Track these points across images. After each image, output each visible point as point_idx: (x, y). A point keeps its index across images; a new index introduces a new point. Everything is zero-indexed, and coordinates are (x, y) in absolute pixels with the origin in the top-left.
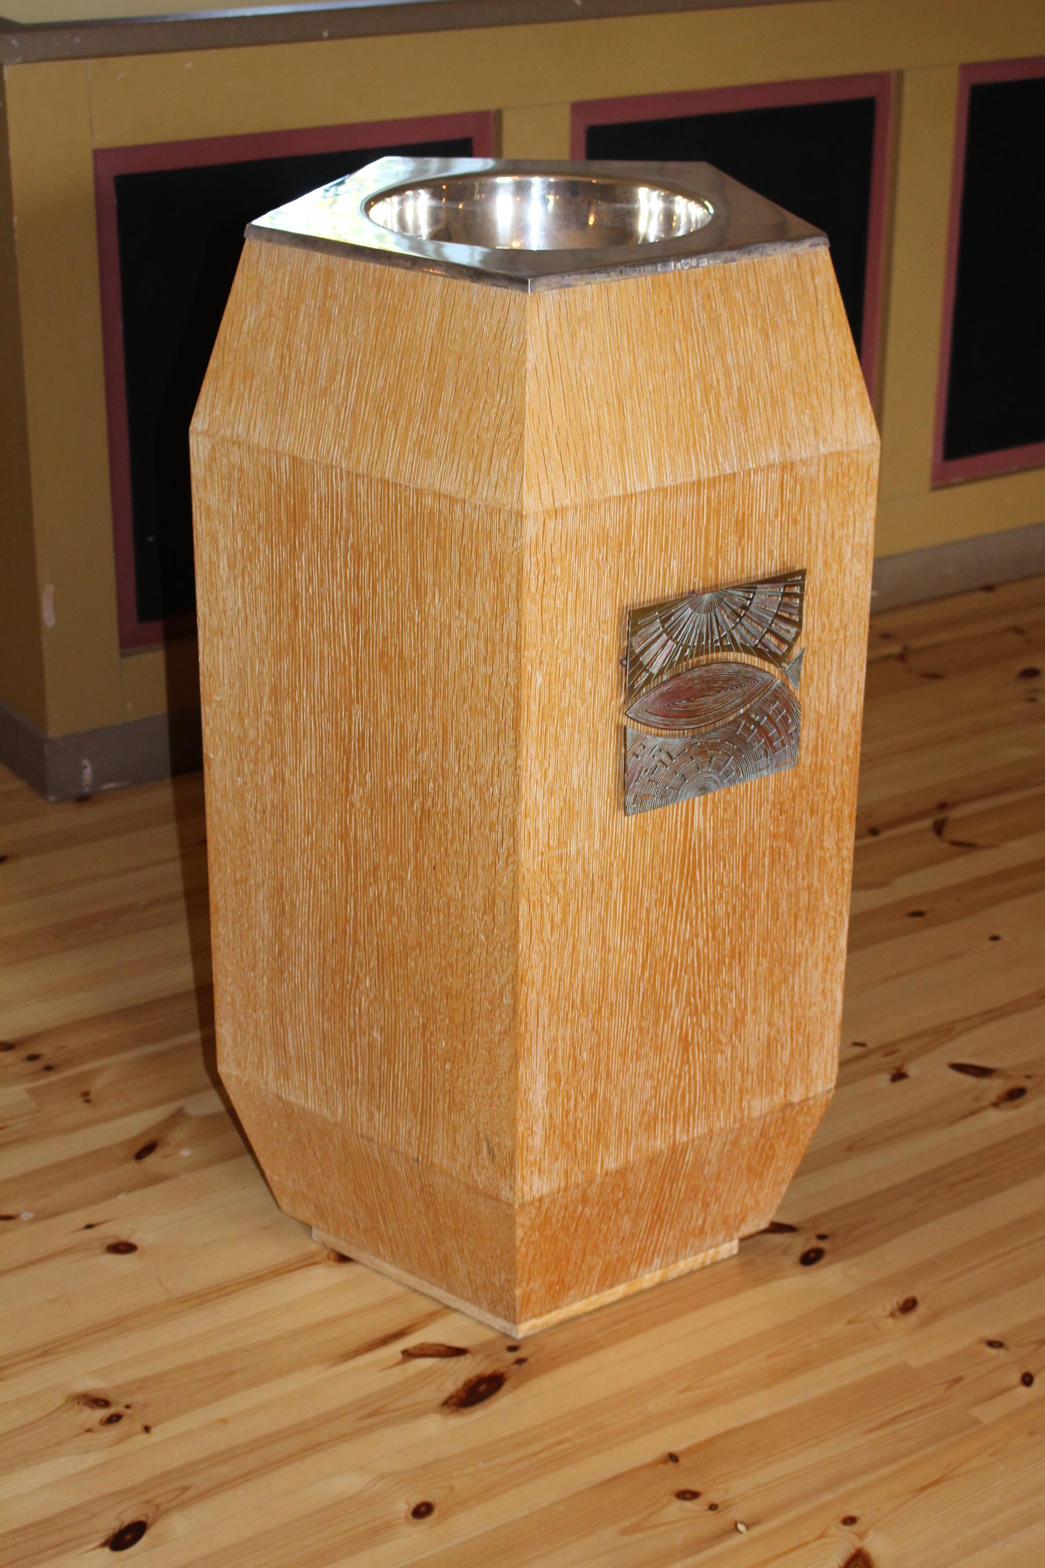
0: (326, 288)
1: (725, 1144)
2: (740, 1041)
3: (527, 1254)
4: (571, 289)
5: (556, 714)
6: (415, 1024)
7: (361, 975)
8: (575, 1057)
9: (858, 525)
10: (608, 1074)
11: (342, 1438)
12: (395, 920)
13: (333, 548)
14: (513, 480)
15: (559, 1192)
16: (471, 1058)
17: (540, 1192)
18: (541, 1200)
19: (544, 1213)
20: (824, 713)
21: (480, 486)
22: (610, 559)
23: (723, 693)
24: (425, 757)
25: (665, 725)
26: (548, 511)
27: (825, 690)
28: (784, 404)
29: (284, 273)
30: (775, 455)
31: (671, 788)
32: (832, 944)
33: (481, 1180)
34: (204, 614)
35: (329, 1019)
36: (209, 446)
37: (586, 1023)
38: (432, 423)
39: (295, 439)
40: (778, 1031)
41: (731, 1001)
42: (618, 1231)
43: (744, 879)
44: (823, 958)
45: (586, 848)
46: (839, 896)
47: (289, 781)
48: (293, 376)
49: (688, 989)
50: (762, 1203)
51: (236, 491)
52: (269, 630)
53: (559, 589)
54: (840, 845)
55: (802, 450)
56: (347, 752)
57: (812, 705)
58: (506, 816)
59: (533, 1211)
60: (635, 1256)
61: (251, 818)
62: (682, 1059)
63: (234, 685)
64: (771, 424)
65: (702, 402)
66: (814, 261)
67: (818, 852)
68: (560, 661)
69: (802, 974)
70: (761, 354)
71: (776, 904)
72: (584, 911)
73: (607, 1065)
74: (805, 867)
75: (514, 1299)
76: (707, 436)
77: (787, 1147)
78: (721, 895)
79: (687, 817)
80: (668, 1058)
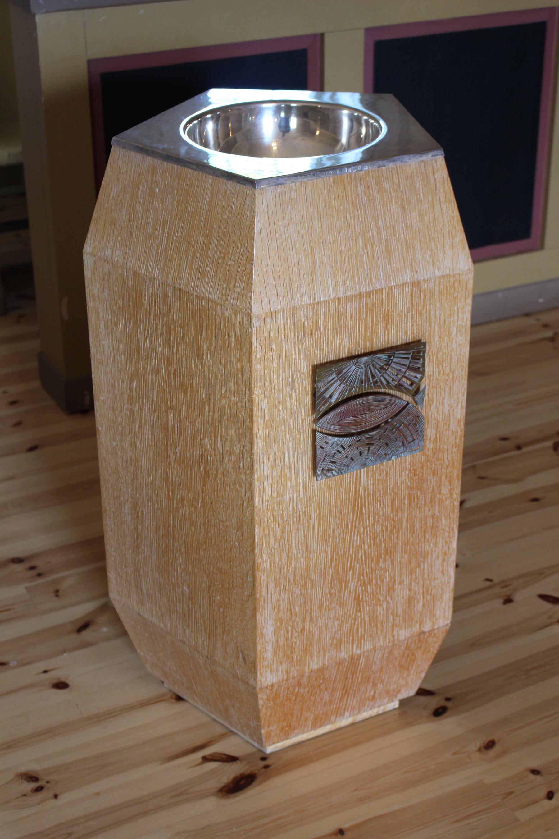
0: (152, 177)
1: (384, 654)
2: (392, 599)
3: (266, 713)
4: (283, 186)
5: (274, 425)
6: (204, 585)
7: (177, 555)
8: (291, 610)
9: (460, 315)
10: (311, 619)
11: (161, 808)
12: (193, 528)
13: (156, 324)
14: (247, 295)
15: (283, 681)
16: (233, 607)
17: (271, 682)
18: (272, 686)
19: (275, 692)
20: (441, 420)
21: (229, 297)
22: (306, 338)
23: (376, 412)
24: (205, 443)
25: (340, 430)
26: (267, 313)
27: (441, 407)
28: (414, 248)
29: (131, 167)
30: (408, 278)
31: (344, 465)
32: (447, 545)
33: (239, 672)
34: (93, 352)
35: (162, 577)
36: (93, 261)
37: (297, 591)
38: (205, 259)
39: (136, 261)
40: (415, 593)
41: (386, 578)
42: (322, 700)
43: (392, 512)
44: (442, 554)
45: (295, 498)
46: (451, 520)
47: (139, 447)
48: (135, 225)
49: (359, 572)
50: (410, 683)
51: (107, 287)
52: (126, 364)
53: (274, 356)
54: (452, 492)
55: (424, 274)
56: (167, 435)
57: (433, 416)
58: (247, 480)
59: (268, 691)
60: (333, 712)
61: (121, 465)
62: (356, 609)
63: (110, 392)
64: (405, 260)
65: (363, 248)
66: (435, 165)
67: (438, 496)
68: (276, 395)
69: (429, 562)
70: (400, 220)
71: (413, 526)
72: (295, 532)
73: (310, 613)
74: (430, 505)
75: (261, 734)
76: (366, 268)
77: (423, 654)
78: (379, 521)
79: (356, 479)
80: (348, 609)
